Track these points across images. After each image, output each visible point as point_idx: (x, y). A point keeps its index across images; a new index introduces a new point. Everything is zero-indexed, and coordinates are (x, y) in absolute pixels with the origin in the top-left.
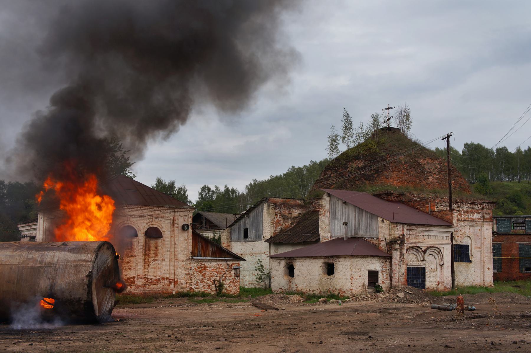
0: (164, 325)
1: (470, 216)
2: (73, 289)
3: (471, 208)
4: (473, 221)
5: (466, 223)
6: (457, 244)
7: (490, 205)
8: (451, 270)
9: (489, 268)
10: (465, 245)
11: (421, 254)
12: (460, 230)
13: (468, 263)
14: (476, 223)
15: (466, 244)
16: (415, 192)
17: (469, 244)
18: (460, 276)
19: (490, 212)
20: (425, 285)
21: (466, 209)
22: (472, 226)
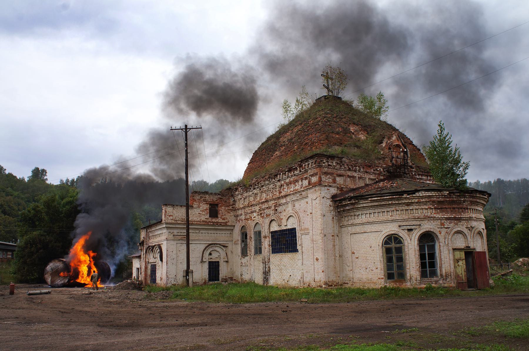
0: (286, 318)
1: (292, 188)
2: (501, 270)
3: (292, 176)
4: (296, 192)
5: (288, 199)
6: (281, 229)
7: (310, 162)
8: (208, 270)
9: (318, 258)
10: (291, 229)
11: (479, 205)
12: (285, 210)
13: (294, 254)
14: (301, 194)
15: (292, 227)
16: (108, 261)
17: (295, 227)
18: (285, 272)
19: (316, 172)
20: (156, 282)
21: (287, 181)
22: (297, 200)
